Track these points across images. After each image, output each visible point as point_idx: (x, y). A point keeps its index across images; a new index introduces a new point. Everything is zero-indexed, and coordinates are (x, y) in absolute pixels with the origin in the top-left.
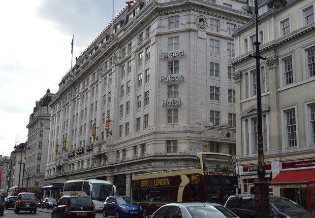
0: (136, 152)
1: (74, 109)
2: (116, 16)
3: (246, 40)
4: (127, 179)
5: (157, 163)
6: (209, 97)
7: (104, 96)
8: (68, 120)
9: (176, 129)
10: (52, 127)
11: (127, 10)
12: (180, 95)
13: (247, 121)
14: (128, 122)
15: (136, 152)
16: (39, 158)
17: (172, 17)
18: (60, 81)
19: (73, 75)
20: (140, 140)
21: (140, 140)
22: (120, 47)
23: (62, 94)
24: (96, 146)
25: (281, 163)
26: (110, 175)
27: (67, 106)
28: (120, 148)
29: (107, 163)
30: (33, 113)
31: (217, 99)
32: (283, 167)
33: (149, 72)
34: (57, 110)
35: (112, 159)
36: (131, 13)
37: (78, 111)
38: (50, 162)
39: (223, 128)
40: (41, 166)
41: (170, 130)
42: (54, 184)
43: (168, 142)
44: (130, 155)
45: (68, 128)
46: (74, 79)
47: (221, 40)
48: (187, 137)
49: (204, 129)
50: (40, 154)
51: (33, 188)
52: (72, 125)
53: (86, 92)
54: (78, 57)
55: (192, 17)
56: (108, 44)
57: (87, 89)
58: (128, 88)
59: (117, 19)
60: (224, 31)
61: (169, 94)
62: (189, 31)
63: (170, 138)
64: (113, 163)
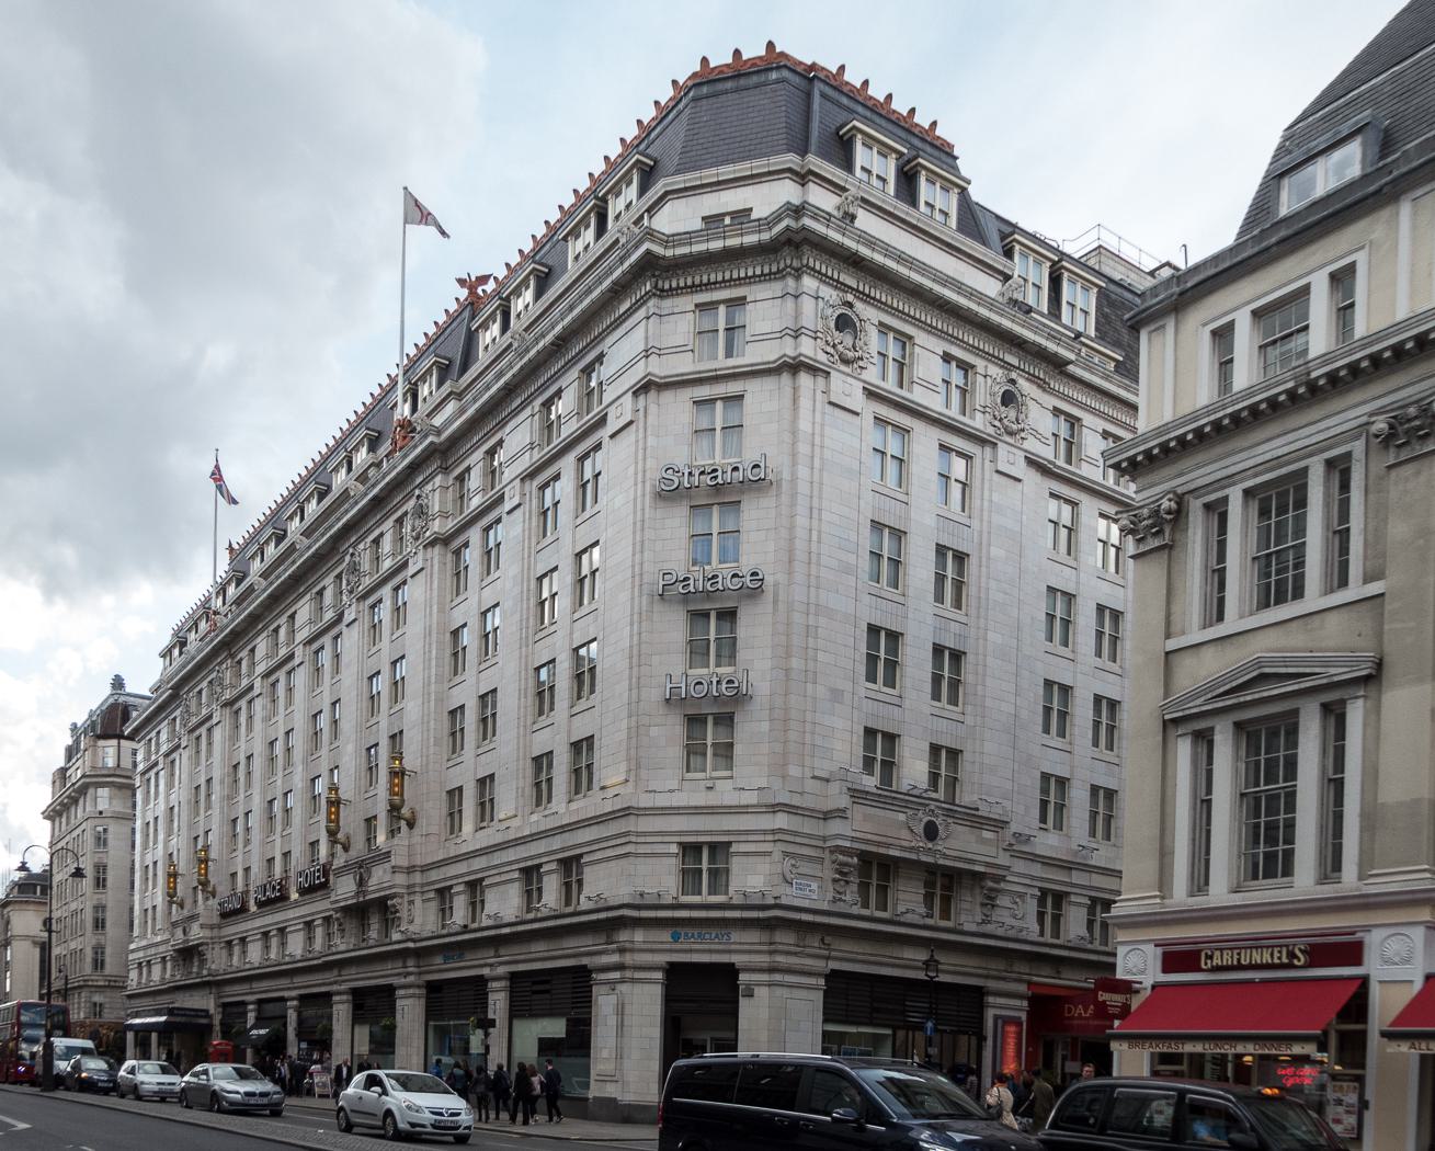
0: (310, 939)
1: (234, 736)
2: (417, 334)
3: (1223, 335)
4: (492, 997)
5: (639, 936)
6: (862, 669)
7: (315, 716)
8: (209, 781)
9: (726, 794)
10: (144, 812)
11: (466, 314)
12: (741, 655)
13: (1204, 739)
14: (492, 777)
15: (310, 939)
16: (99, 924)
17: (713, 305)
18: (166, 640)
19: (223, 610)
20: (556, 843)
21: (556, 843)
22: (446, 470)
23: (175, 692)
24: (340, 872)
25: (1159, 951)
26: (411, 979)
27: (203, 730)
28: (456, 877)
29: (396, 936)
30: (61, 763)
31: (890, 682)
32: (1166, 969)
33: (403, 669)
34: (164, 748)
35: (420, 920)
36: (492, 317)
37: (254, 743)
38: (143, 935)
39: (908, 801)
40: (108, 951)
41: (702, 803)
42: (171, 1012)
43: (690, 850)
44: (504, 904)
45: (216, 811)
46: (229, 622)
47: (918, 426)
48: (773, 832)
49: (844, 801)
50: (100, 908)
51: (82, 1025)
52: (230, 798)
53: (207, 725)
54: (238, 539)
55: (807, 304)
56: (378, 465)
57: (291, 657)
58: (397, 685)
59: (422, 352)
60: (929, 386)
61: (697, 651)
62: (794, 367)
63: (697, 833)
64: (425, 935)
